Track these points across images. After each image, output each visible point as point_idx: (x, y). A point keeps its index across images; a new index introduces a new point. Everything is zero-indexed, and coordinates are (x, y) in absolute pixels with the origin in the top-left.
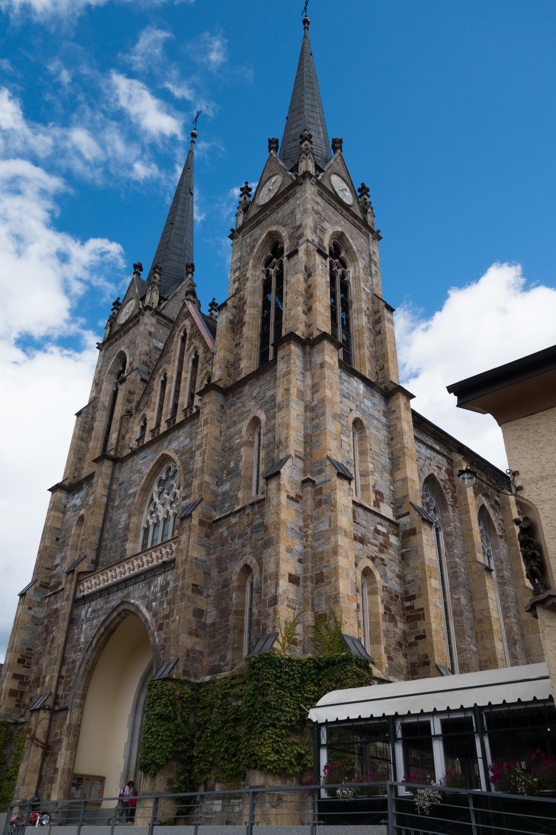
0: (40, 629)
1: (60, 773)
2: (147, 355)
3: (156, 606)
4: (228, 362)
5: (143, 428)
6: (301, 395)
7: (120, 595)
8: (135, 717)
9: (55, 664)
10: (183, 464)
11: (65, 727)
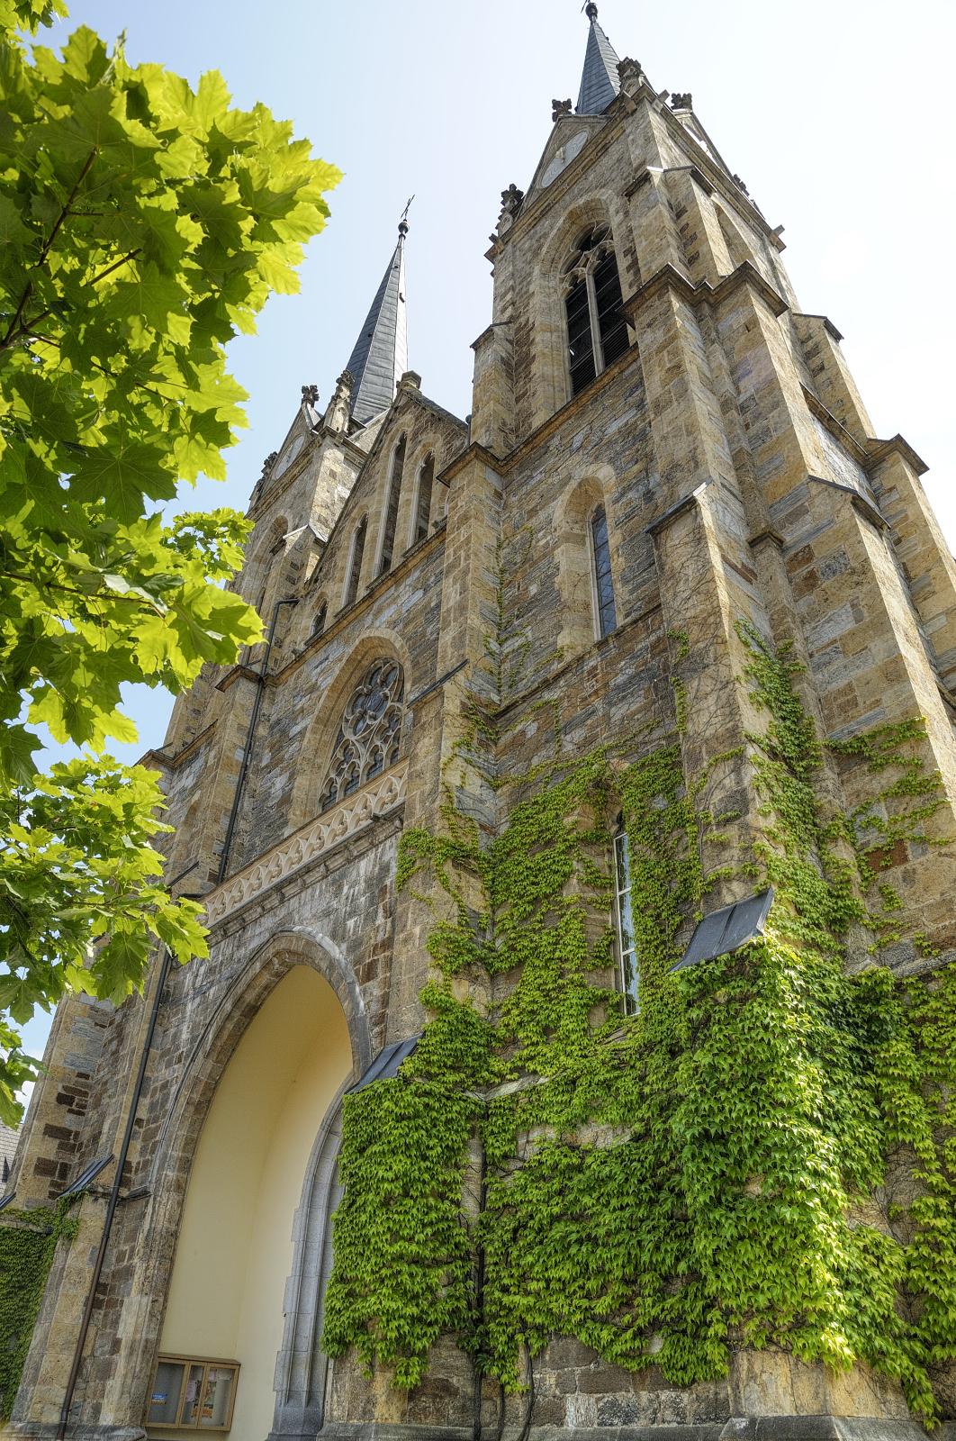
0: (107, 1033)
1: (123, 1352)
4: (504, 424)
6: (710, 385)
7: (269, 922)
8: (309, 1216)
9: (124, 1092)
11: (141, 1237)
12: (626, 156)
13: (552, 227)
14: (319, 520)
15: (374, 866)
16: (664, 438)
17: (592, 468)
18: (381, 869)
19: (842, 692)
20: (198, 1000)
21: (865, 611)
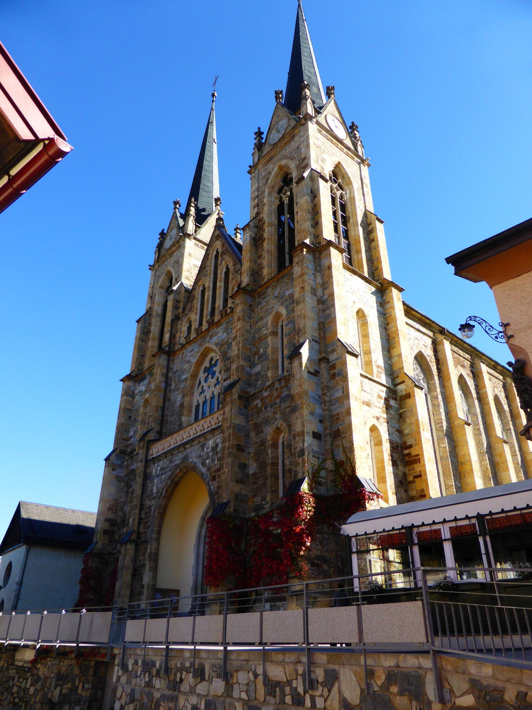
1: (146, 588)
2: (189, 271)
5: (189, 328)
7: (180, 456)
10: (222, 353)
11: (147, 555)
14: (186, 278)
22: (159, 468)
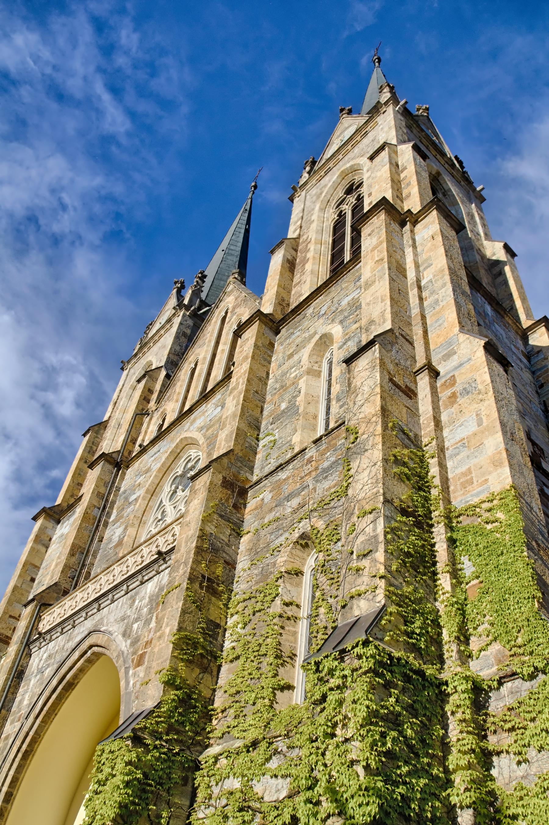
3: (138, 628)
7: (89, 625)
12: (377, 138)
13: (330, 181)
15: (156, 587)
16: (368, 304)
17: (330, 327)
18: (159, 589)
19: (464, 474)
20: (38, 677)
21: (484, 418)
22: (45, 655)
